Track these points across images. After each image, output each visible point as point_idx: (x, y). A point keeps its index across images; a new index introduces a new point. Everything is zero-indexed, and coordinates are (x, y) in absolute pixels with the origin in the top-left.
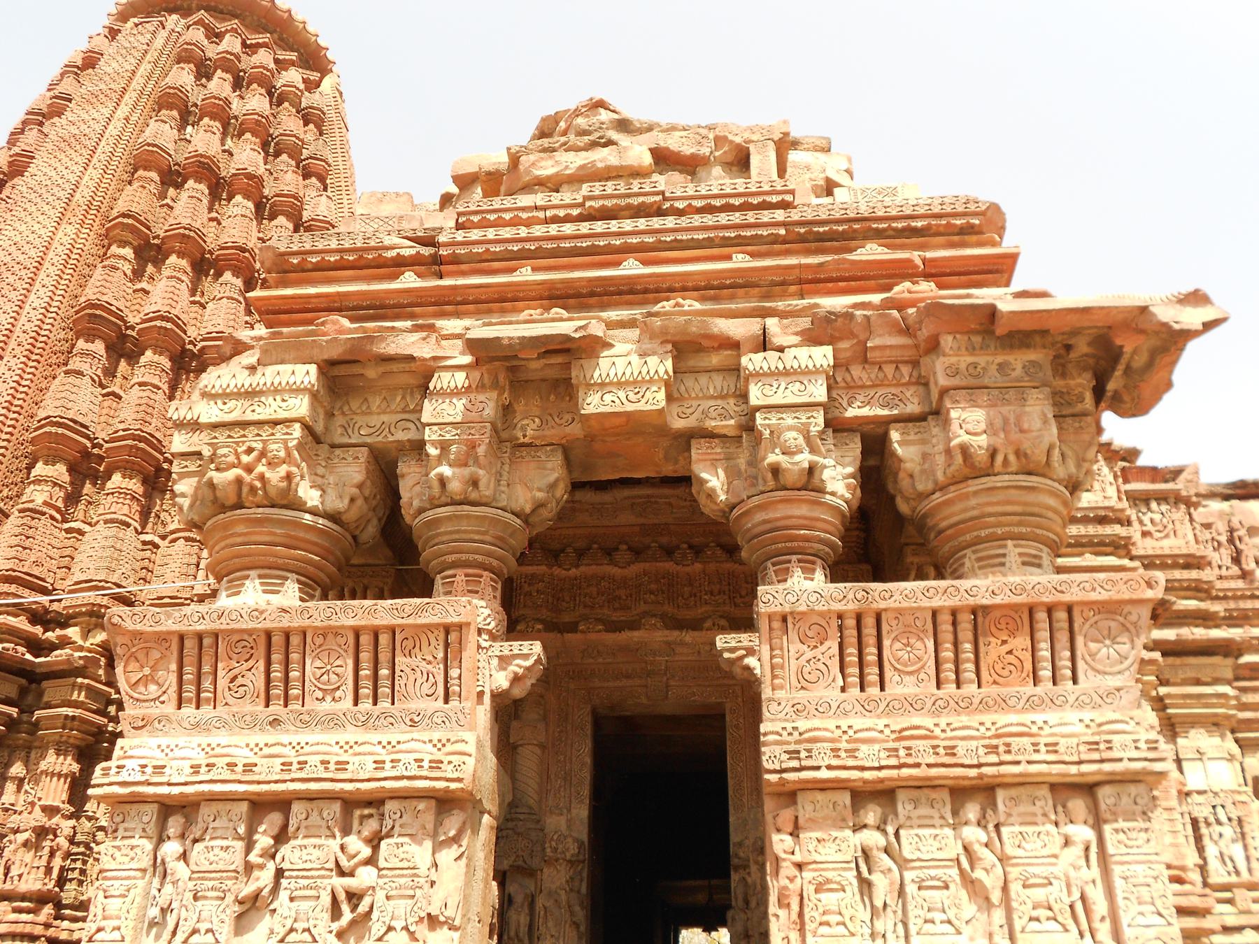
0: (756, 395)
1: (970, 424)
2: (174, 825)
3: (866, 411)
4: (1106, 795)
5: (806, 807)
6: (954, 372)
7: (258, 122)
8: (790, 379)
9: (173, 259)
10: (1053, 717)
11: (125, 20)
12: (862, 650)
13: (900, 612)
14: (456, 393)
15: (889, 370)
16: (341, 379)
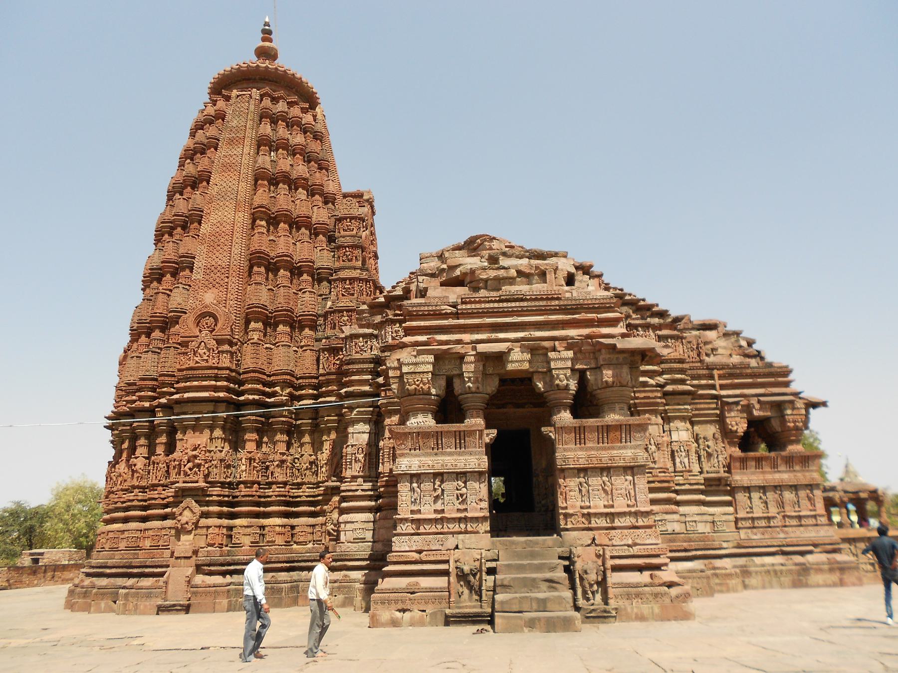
0: (553, 365)
1: (608, 375)
3: (581, 367)
4: (635, 470)
5: (567, 474)
6: (604, 360)
7: (302, 149)
8: (562, 363)
9: (282, 225)
10: (624, 451)
12: (580, 434)
13: (589, 427)
14: (471, 363)
15: (587, 355)
16: (440, 357)
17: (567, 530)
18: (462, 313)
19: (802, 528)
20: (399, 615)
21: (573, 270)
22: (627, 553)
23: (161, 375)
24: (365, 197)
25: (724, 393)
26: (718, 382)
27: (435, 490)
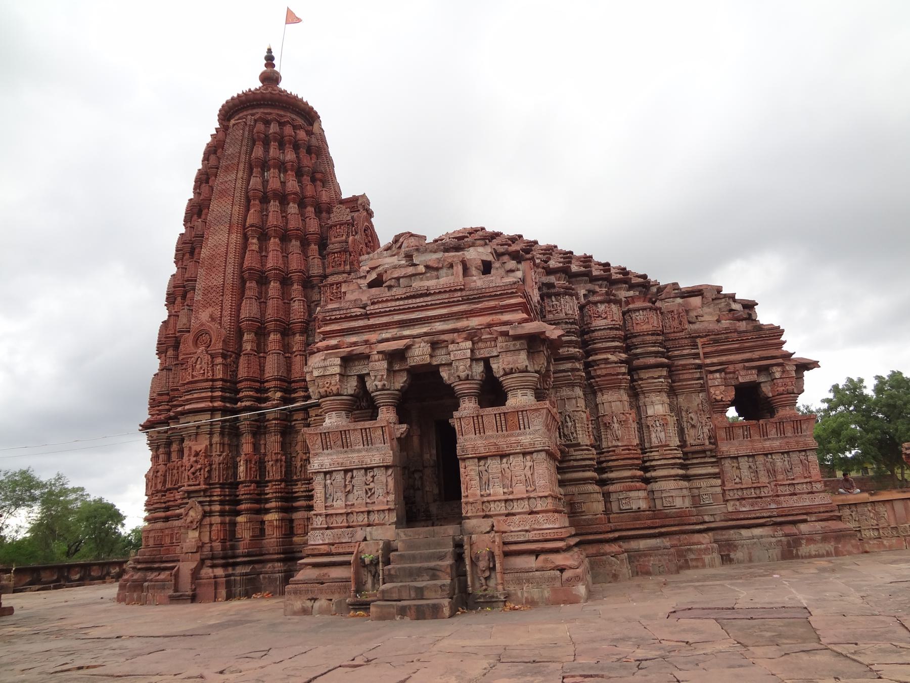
2: (328, 476)
11: (229, 120)
16: (347, 361)
17: (468, 518)
18: (371, 314)
19: (795, 497)
20: (309, 604)
21: (490, 258)
22: (522, 539)
23: (172, 390)
24: (359, 202)
25: (708, 361)
26: (701, 351)
27: (345, 486)
